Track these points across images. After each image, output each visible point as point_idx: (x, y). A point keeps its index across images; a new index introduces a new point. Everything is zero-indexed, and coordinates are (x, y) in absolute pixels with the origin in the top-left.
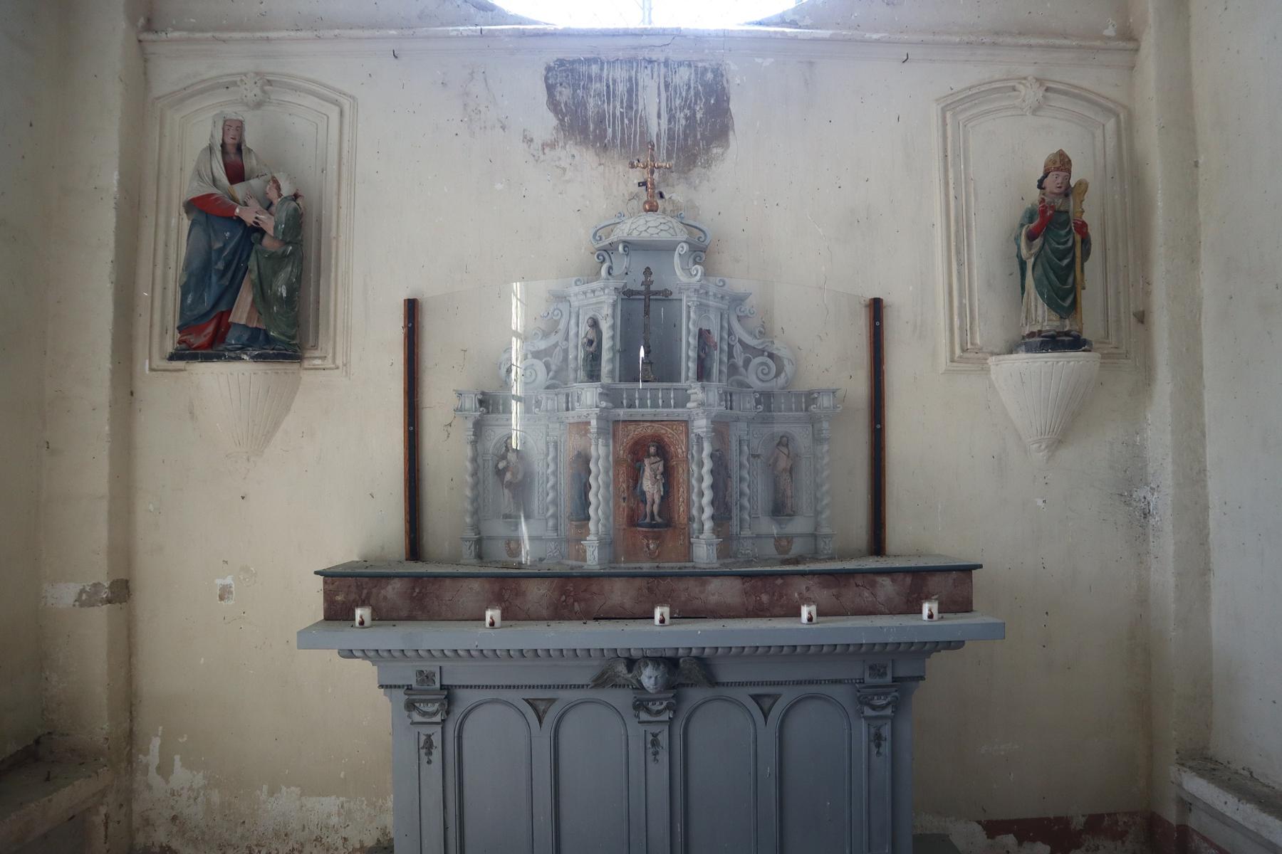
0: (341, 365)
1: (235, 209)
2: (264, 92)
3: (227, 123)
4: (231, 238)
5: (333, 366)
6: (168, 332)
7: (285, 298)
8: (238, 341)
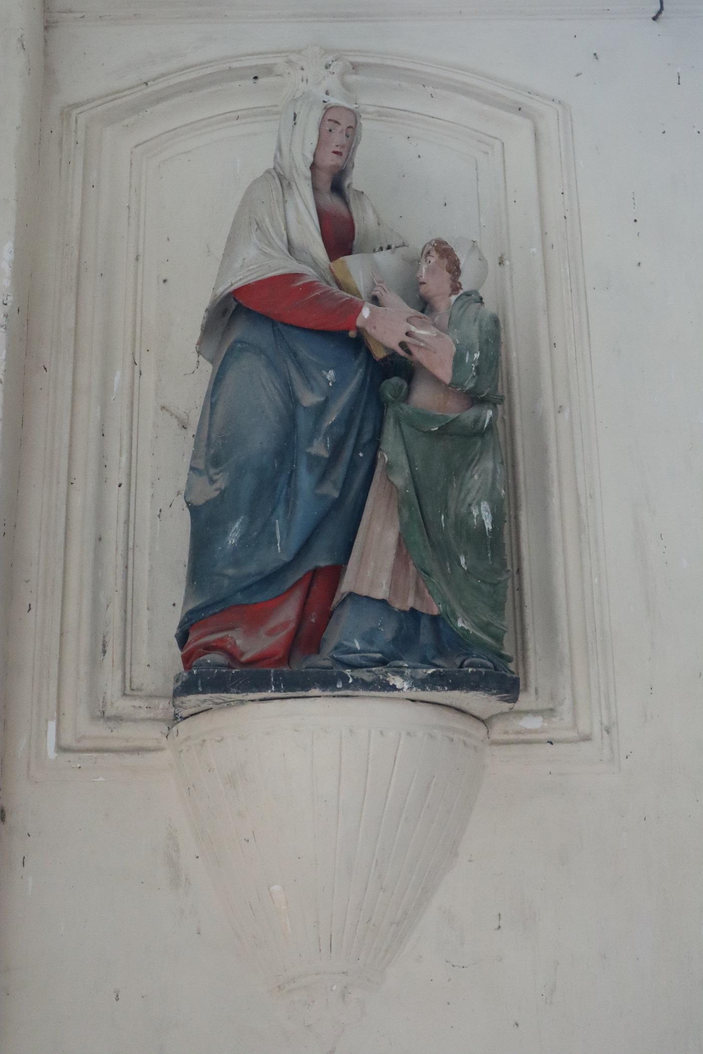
0: (597, 730)
1: (359, 310)
2: (346, 87)
3: (329, 117)
4: (339, 385)
5: (572, 734)
6: (109, 649)
7: (491, 529)
8: (371, 643)
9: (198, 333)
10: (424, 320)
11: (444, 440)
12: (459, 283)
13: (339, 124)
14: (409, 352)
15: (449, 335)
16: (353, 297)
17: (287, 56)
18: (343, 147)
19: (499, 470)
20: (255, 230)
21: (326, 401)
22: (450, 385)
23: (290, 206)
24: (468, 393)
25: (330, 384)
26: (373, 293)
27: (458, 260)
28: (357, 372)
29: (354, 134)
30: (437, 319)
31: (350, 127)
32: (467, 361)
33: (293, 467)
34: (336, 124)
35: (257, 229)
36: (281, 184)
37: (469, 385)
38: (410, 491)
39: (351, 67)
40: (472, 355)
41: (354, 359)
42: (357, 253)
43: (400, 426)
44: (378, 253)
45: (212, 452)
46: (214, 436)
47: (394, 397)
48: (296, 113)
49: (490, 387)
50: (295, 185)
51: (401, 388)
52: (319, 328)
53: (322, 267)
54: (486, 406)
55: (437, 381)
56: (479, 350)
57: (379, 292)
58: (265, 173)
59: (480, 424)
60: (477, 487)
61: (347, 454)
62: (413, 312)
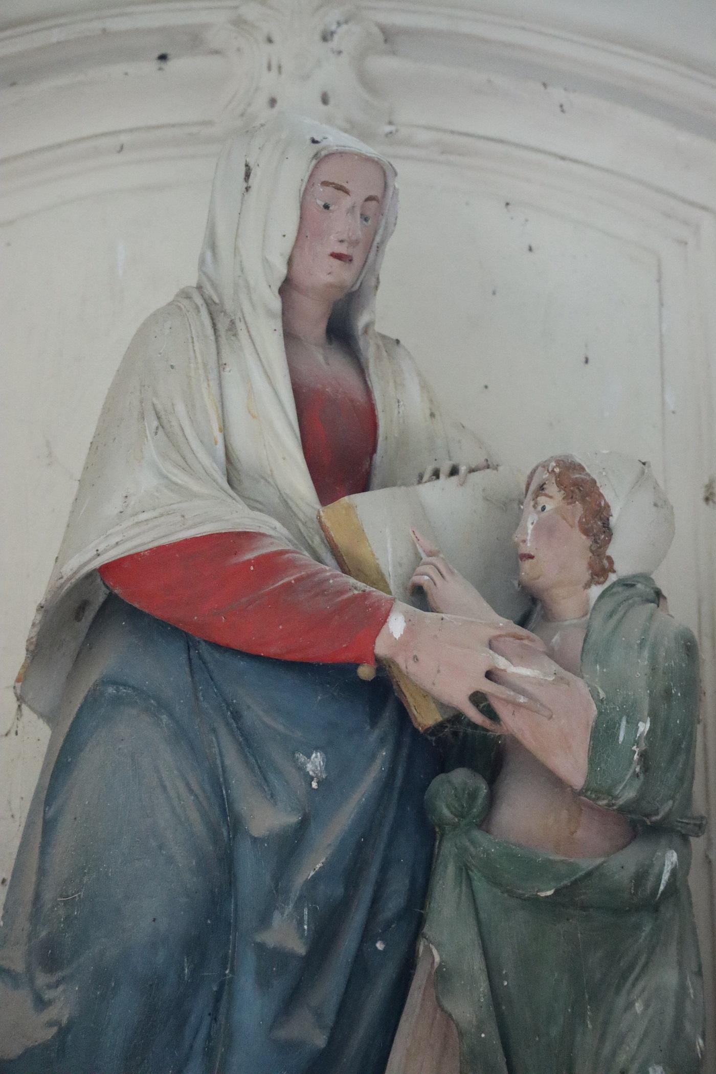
1: (383, 620)
2: (367, 82)
9: (20, 657)
10: (526, 642)
11: (568, 920)
12: (609, 559)
13: (347, 192)
14: (490, 713)
15: (583, 678)
16: (368, 589)
17: (236, 8)
18: (354, 243)
19: (691, 991)
20: (154, 430)
21: (304, 824)
22: (583, 792)
23: (231, 376)
24: (622, 810)
25: (314, 785)
26: (416, 579)
27: (607, 506)
28: (373, 757)
29: (380, 212)
30: (556, 639)
31: (370, 199)
32: (621, 739)
33: (225, 975)
34: (341, 193)
35: (157, 428)
36: (214, 326)
37: (627, 794)
38: (490, 1035)
39: (381, 38)
40: (633, 724)
41: (368, 728)
42: (384, 485)
43: (469, 879)
44: (428, 484)
45: (43, 934)
46: (48, 896)
47: (456, 816)
48: (251, 165)
49: (672, 798)
50: (244, 327)
51: (473, 796)
52: (289, 657)
53: (301, 516)
54: (663, 842)
55: (556, 782)
56: (649, 715)
57: (426, 578)
58: (177, 295)
59: (650, 885)
60: (641, 1028)
61: (348, 944)
62: (505, 624)
